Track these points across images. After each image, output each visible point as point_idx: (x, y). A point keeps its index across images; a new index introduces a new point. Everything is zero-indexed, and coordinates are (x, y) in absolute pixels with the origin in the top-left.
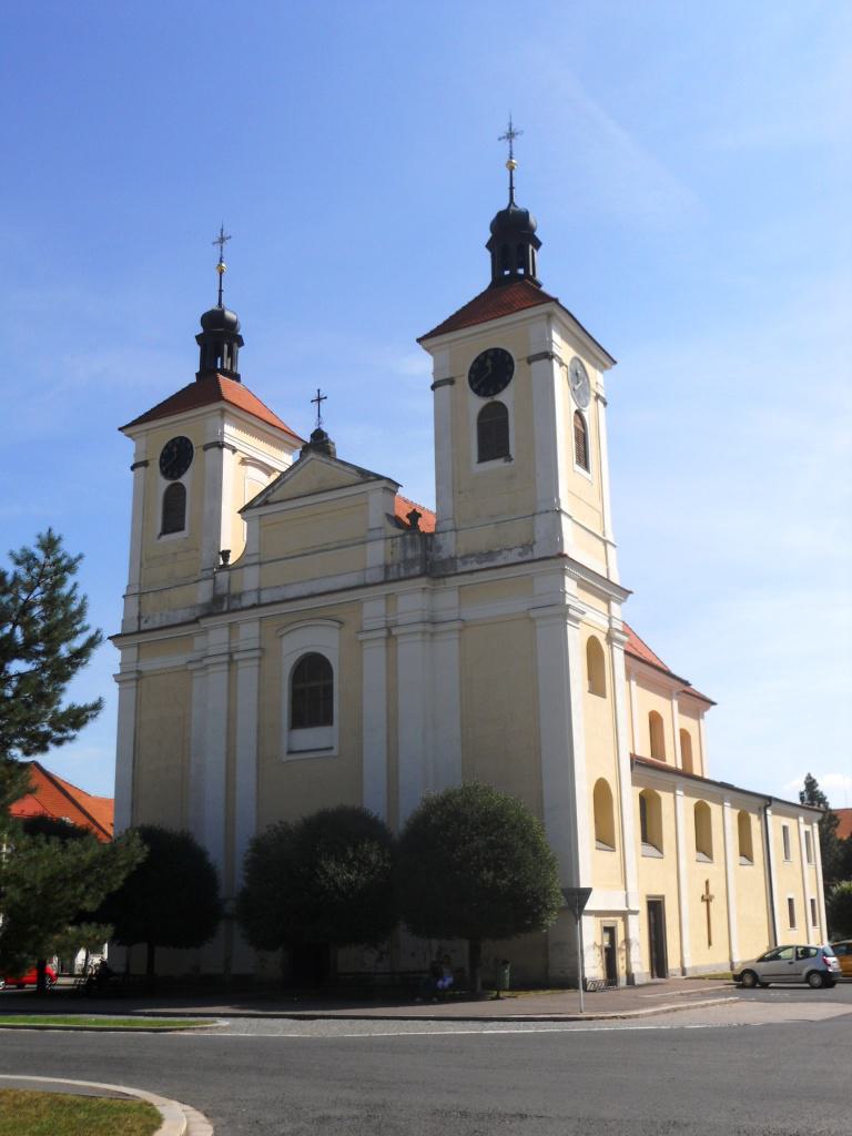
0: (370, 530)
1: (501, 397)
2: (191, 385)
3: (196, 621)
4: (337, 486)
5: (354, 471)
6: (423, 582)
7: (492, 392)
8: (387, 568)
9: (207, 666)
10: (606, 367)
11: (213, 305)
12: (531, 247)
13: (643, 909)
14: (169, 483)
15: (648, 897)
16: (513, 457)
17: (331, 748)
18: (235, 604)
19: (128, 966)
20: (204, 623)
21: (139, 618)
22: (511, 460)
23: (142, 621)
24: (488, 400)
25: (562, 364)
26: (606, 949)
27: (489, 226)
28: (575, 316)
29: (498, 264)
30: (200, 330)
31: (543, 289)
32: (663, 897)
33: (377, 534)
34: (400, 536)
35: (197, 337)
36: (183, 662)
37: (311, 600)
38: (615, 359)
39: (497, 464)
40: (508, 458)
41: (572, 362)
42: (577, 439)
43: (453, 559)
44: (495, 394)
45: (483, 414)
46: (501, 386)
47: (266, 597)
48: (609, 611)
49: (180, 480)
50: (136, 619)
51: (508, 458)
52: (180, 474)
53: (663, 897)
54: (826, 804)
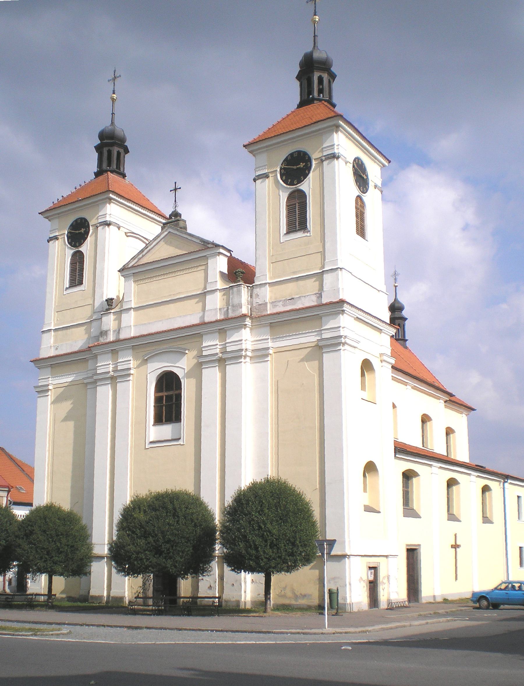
5: (198, 241)
9: (95, 382)
26: (371, 582)
27: (489, 485)
32: (419, 545)
39: (300, 234)
42: (357, 216)
46: (302, 178)
49: (80, 249)
52: (81, 244)
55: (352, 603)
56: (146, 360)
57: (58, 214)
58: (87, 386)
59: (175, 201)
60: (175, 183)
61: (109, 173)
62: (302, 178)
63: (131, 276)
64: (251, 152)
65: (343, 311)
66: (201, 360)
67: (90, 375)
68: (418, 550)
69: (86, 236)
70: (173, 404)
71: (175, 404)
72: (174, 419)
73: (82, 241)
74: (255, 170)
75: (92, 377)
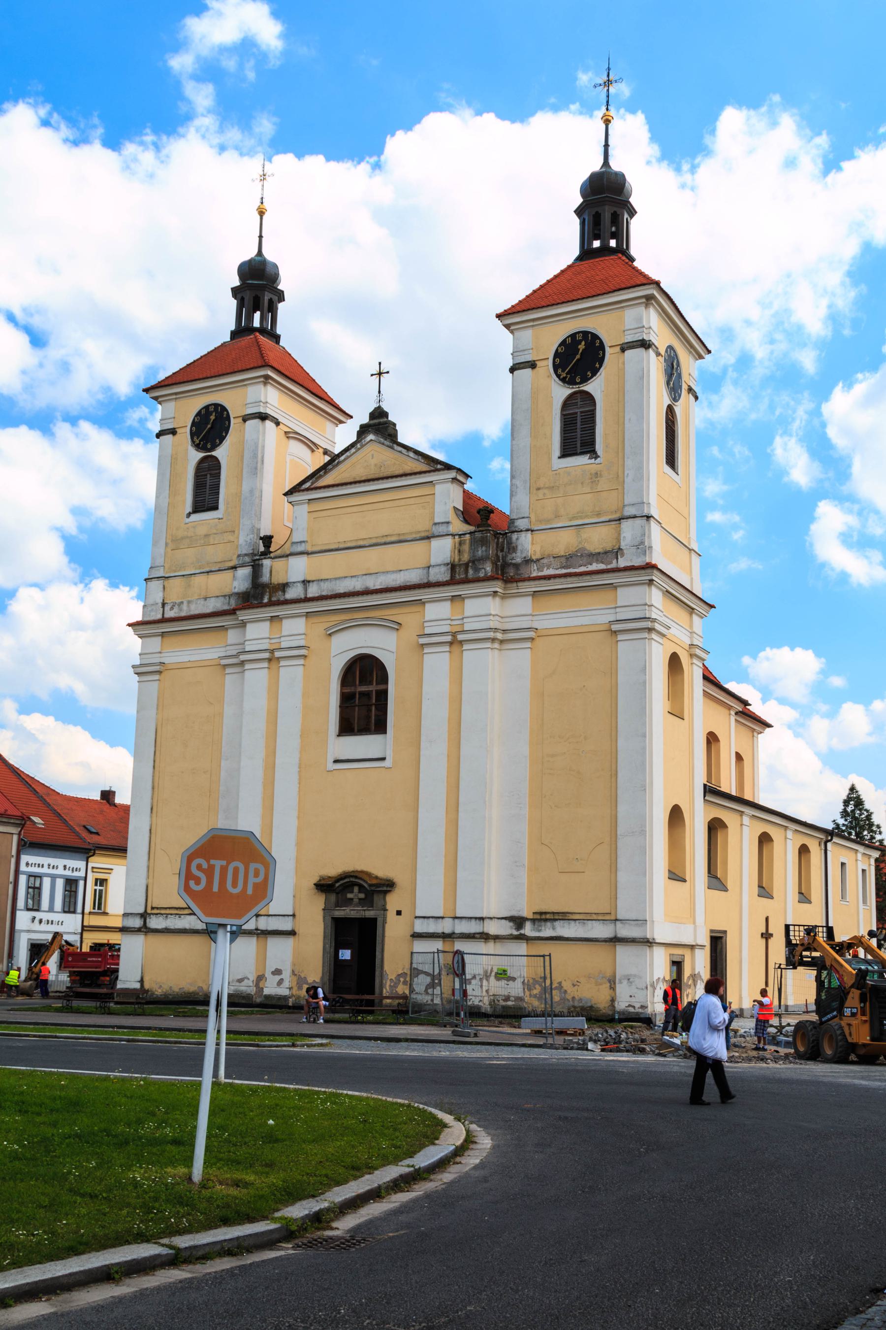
0: (435, 524)
1: (589, 387)
2: (224, 345)
3: (232, 612)
4: (397, 473)
6: (498, 586)
7: (578, 380)
8: (453, 567)
9: (242, 663)
10: (701, 357)
11: (250, 253)
12: (626, 216)
13: (707, 942)
14: (201, 455)
15: (712, 931)
16: (599, 453)
17: (383, 759)
18: (279, 596)
19: (142, 981)
20: (243, 615)
21: (164, 605)
22: (597, 457)
23: (167, 608)
24: (575, 389)
25: (658, 354)
28: (706, 343)
29: (588, 233)
30: (237, 282)
31: (635, 264)
32: (725, 932)
33: (442, 529)
34: (470, 533)
35: (232, 289)
36: (216, 656)
37: (365, 598)
38: (710, 348)
39: (582, 461)
40: (593, 454)
41: (666, 351)
43: (528, 561)
44: (580, 383)
45: (567, 403)
47: (313, 591)
48: (691, 626)
50: (160, 605)
51: (593, 454)
53: (725, 932)
54: (818, 979)
55: (655, 1014)
56: (330, 635)
57: (176, 394)
58: (225, 669)
59: (379, 392)
60: (380, 364)
61: (258, 334)
62: (589, 373)
63: (304, 503)
64: (507, 326)
65: (651, 581)
66: (423, 641)
67: (234, 653)
68: (724, 938)
69: (224, 434)
70: (371, 705)
71: (375, 705)
72: (373, 728)
73: (218, 441)
74: (512, 354)
75: (236, 656)
